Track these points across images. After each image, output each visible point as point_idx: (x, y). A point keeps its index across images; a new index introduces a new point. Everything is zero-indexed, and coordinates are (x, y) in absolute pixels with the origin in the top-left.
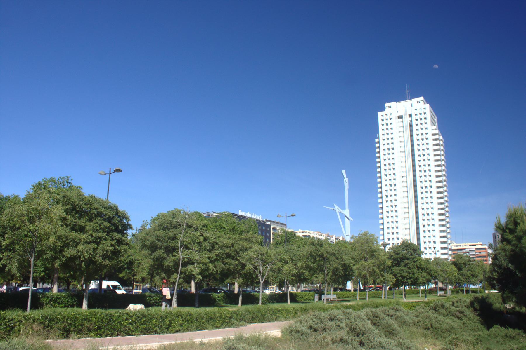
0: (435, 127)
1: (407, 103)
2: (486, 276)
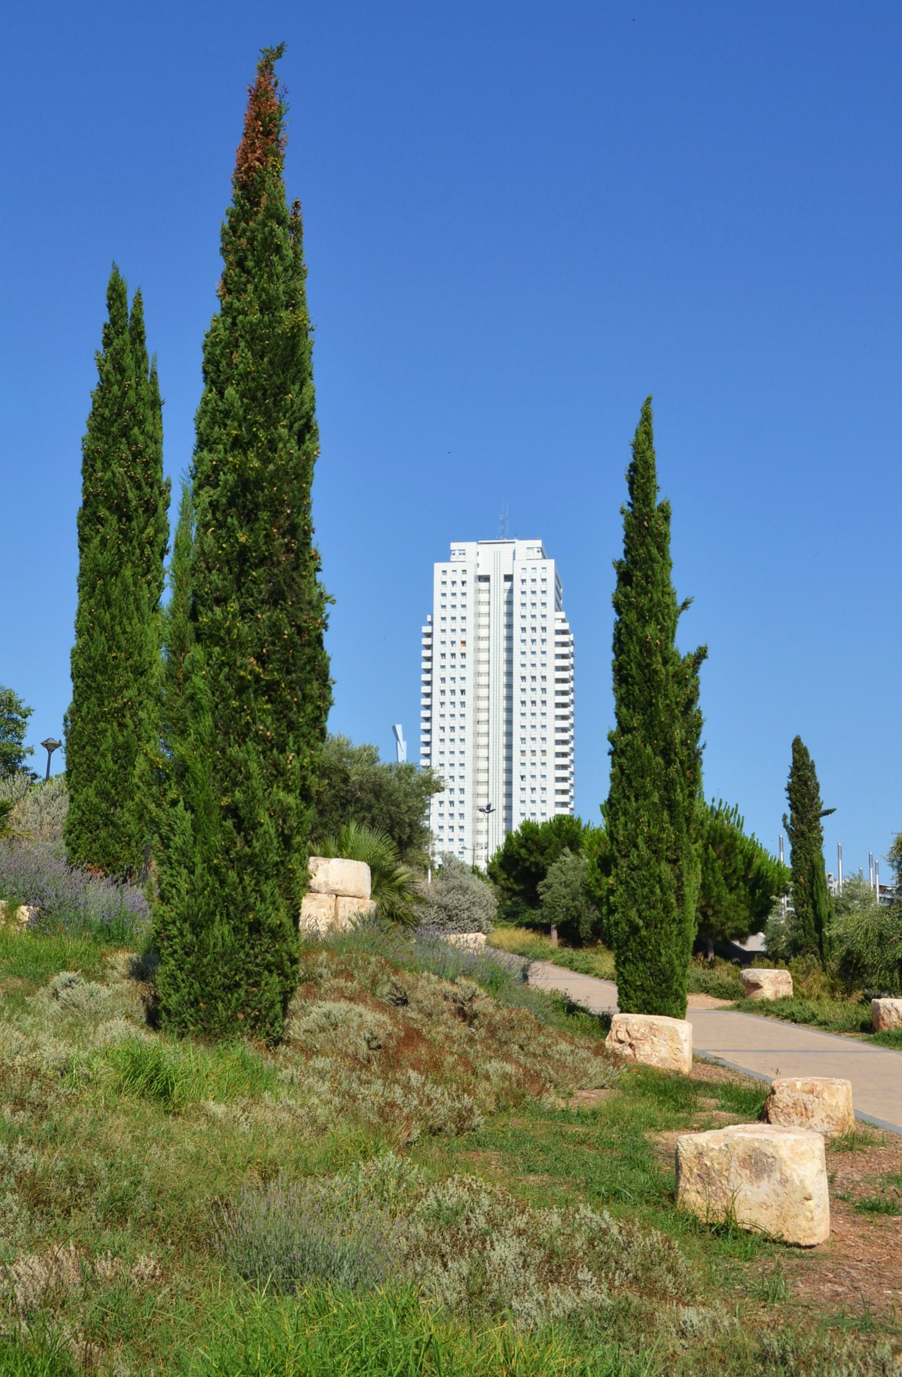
0: (562, 615)
1: (505, 549)
2: (622, 570)
